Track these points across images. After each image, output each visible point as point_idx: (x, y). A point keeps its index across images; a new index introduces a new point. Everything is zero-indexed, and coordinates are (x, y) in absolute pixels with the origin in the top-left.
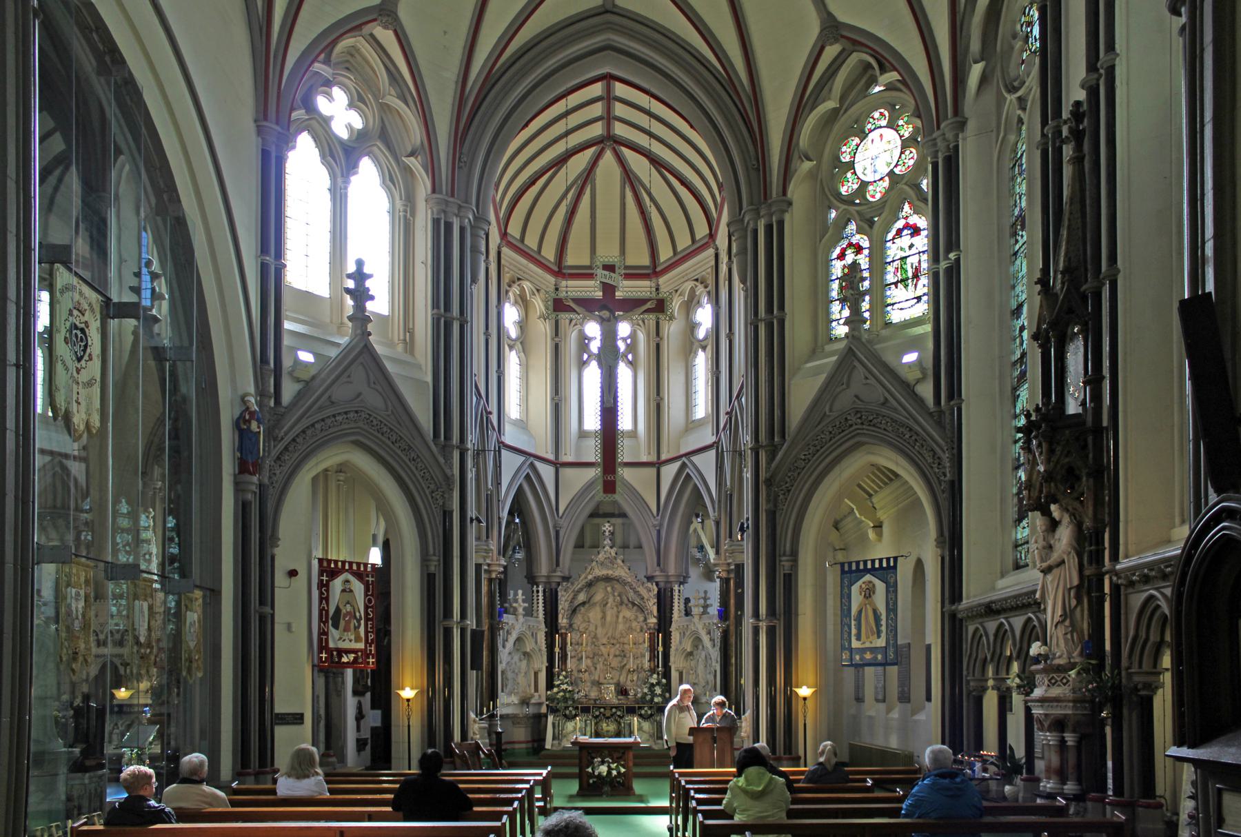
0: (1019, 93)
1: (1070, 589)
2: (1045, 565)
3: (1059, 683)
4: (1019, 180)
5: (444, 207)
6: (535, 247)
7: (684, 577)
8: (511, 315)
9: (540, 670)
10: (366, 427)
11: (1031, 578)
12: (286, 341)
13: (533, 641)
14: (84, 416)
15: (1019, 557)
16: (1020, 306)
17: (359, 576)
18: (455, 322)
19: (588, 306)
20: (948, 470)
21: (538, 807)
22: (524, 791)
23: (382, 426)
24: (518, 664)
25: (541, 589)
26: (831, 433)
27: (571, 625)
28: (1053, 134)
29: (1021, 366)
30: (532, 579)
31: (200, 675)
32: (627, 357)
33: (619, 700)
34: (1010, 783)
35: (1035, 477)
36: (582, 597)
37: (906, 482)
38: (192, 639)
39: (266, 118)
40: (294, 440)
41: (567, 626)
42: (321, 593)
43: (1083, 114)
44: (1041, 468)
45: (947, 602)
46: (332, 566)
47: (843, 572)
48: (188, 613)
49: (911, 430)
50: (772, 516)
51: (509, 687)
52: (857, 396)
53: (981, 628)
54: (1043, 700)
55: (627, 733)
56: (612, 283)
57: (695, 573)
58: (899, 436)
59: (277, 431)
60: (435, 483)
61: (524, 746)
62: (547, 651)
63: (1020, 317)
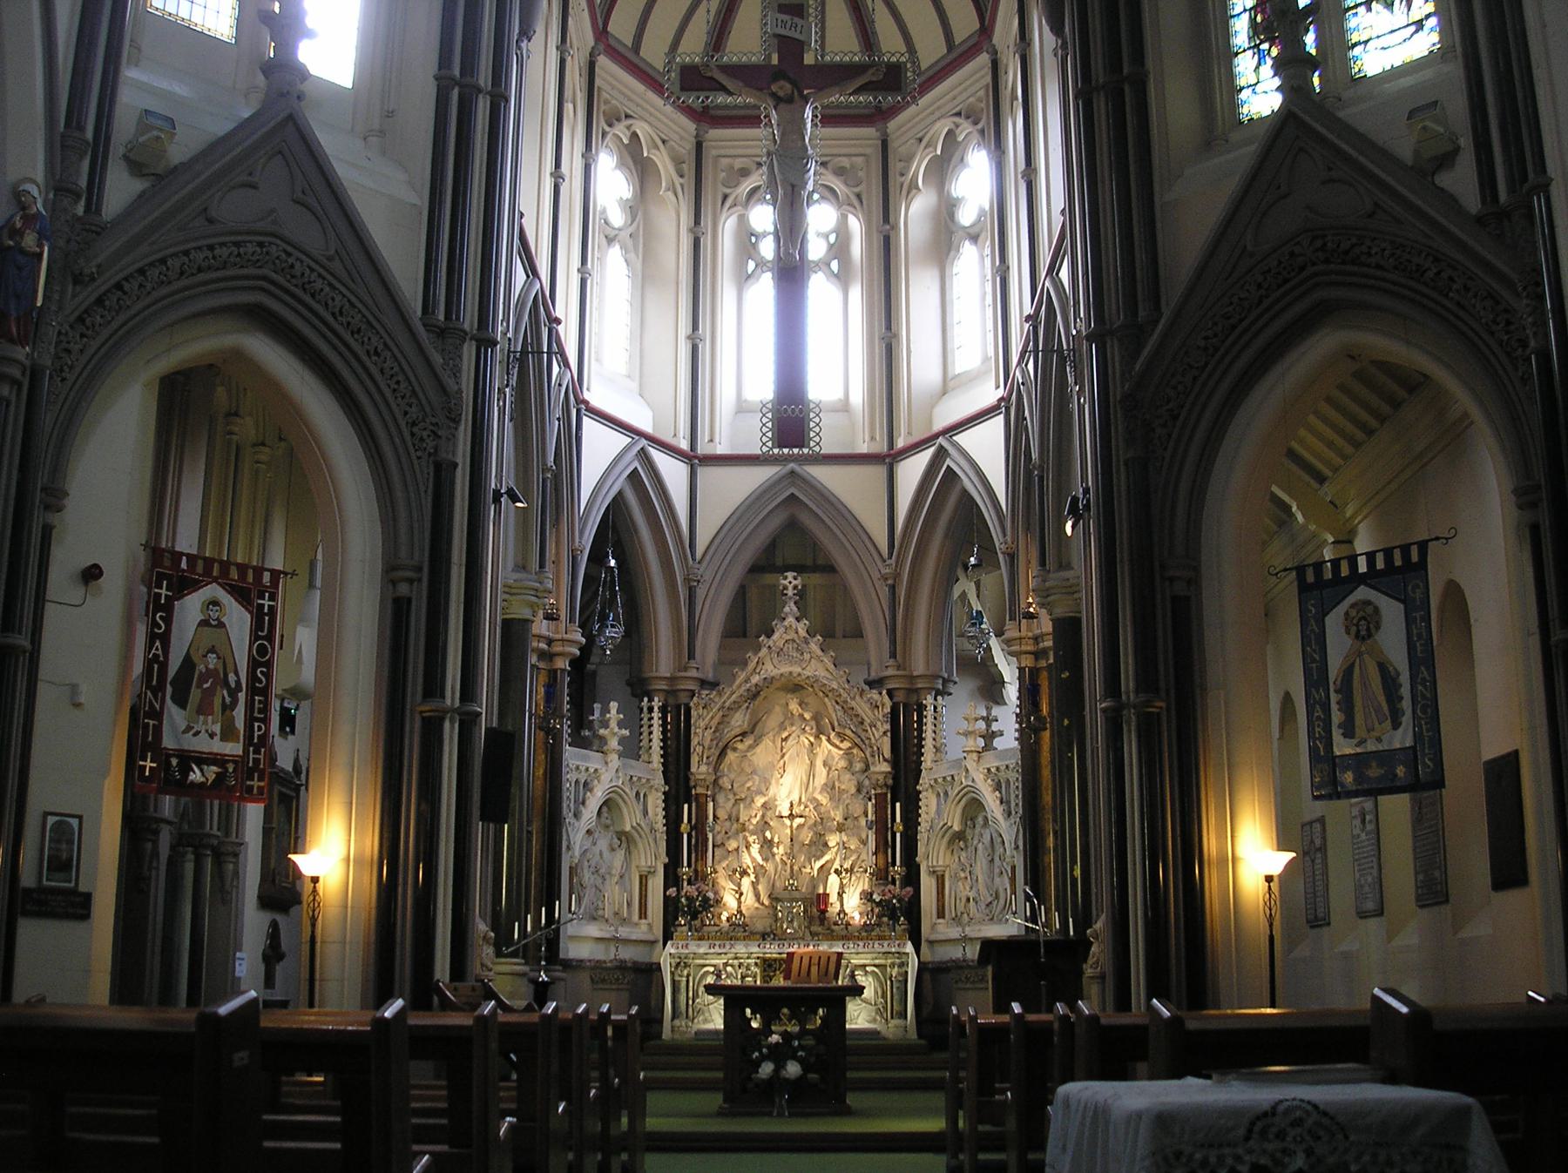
7: (945, 681)
13: (639, 809)
25: (656, 703)
26: (1259, 286)
32: (829, 265)
46: (184, 565)
47: (1304, 588)
56: (797, 36)
62: (668, 833)
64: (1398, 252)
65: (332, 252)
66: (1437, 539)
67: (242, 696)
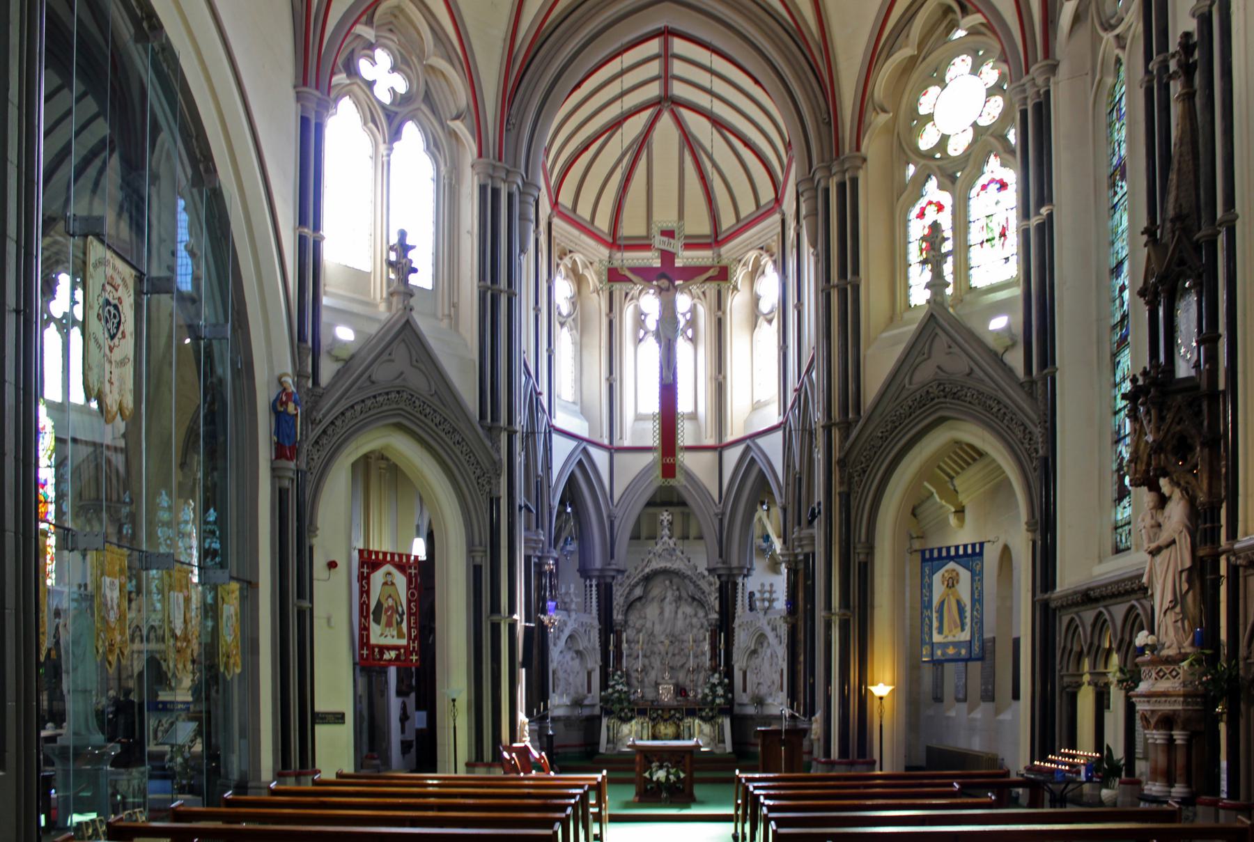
0: (1117, 31)
1: (1181, 572)
2: (1153, 545)
3: (1168, 675)
4: (1117, 126)
5: (491, 171)
6: (588, 217)
7: (749, 570)
8: (563, 289)
9: (593, 670)
10: (408, 409)
11: (1135, 561)
12: (325, 317)
14: (117, 397)
15: (1118, 539)
16: (1120, 264)
17: (402, 567)
18: (502, 295)
19: (646, 274)
20: (1040, 446)
21: (592, 813)
22: (578, 797)
23: (425, 406)
24: (570, 663)
25: (594, 582)
26: (910, 407)
27: (626, 622)
28: (1159, 70)
29: (1121, 330)
30: (584, 573)
31: (238, 670)
33: (677, 701)
34: (1107, 787)
35: (1142, 445)
36: (638, 592)
37: (994, 461)
38: (229, 636)
39: (305, 83)
40: (332, 423)
41: (623, 623)
42: (362, 586)
43: (1194, 45)
44: (1150, 438)
45: (1038, 590)
46: (373, 557)
47: (924, 560)
48: (225, 605)
49: (999, 403)
50: (846, 498)
51: (560, 688)
52: (939, 367)
53: (1077, 618)
54: (1149, 696)
55: (686, 736)
57: (759, 565)
58: (986, 410)
59: (314, 413)
60: (481, 467)
61: (577, 750)
63: (1120, 276)
64: (980, 397)
65: (433, 392)
66: (989, 541)
67: (405, 617)
